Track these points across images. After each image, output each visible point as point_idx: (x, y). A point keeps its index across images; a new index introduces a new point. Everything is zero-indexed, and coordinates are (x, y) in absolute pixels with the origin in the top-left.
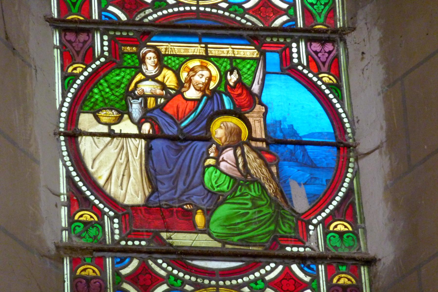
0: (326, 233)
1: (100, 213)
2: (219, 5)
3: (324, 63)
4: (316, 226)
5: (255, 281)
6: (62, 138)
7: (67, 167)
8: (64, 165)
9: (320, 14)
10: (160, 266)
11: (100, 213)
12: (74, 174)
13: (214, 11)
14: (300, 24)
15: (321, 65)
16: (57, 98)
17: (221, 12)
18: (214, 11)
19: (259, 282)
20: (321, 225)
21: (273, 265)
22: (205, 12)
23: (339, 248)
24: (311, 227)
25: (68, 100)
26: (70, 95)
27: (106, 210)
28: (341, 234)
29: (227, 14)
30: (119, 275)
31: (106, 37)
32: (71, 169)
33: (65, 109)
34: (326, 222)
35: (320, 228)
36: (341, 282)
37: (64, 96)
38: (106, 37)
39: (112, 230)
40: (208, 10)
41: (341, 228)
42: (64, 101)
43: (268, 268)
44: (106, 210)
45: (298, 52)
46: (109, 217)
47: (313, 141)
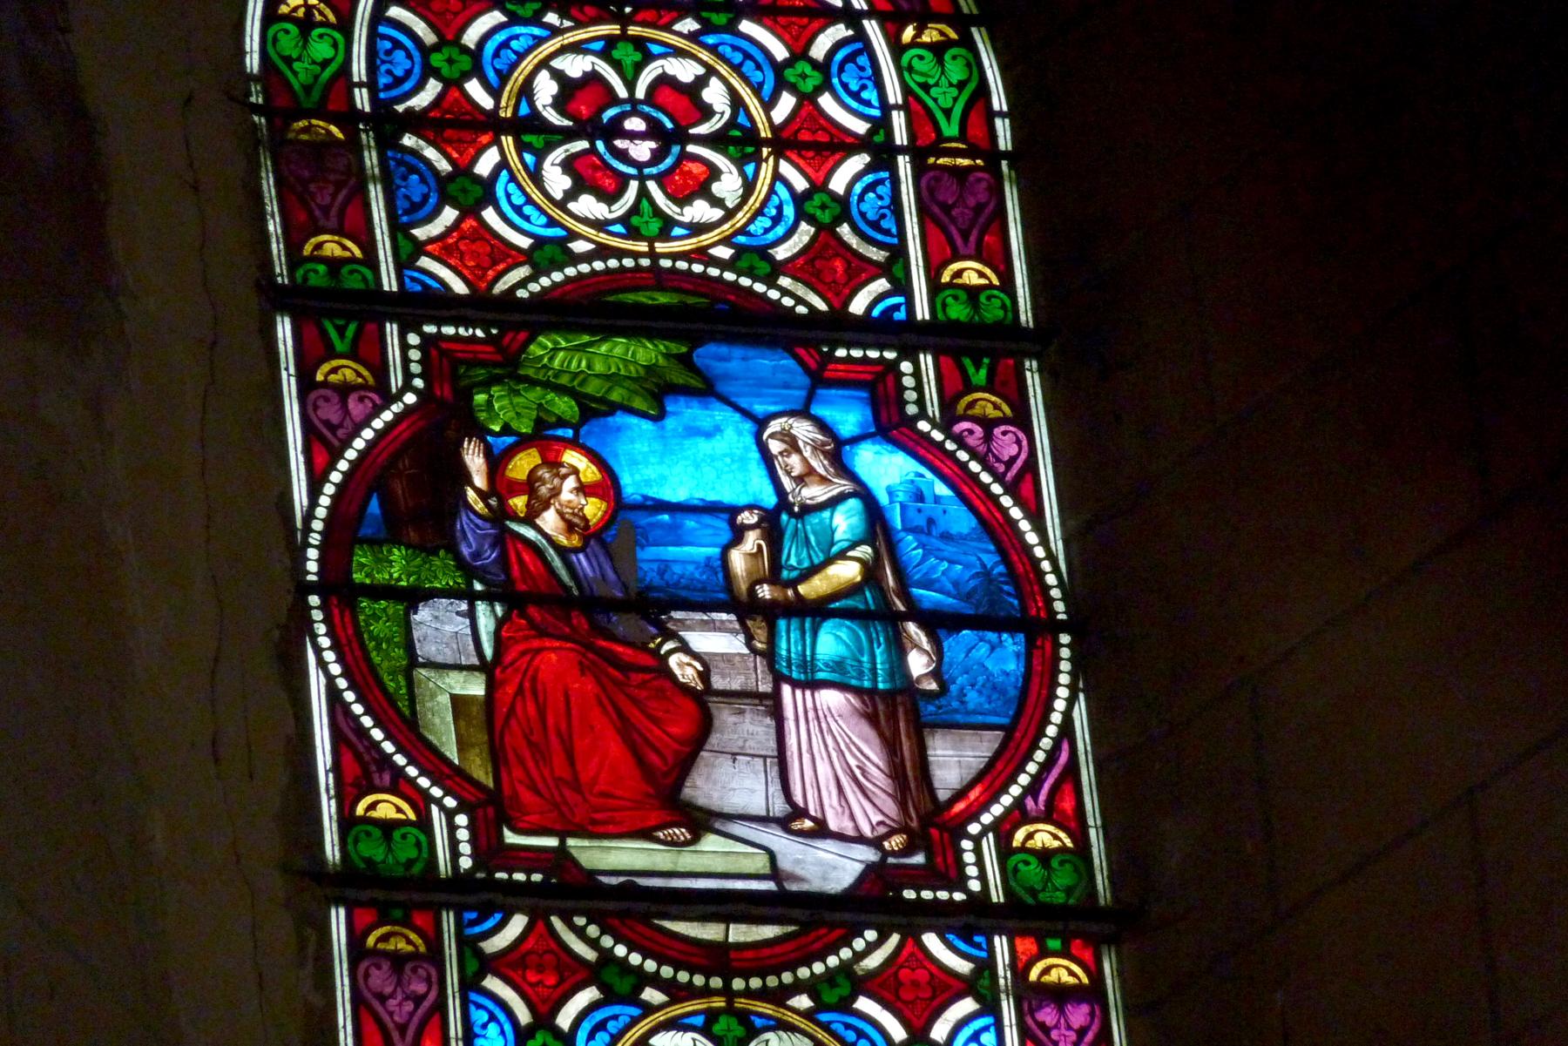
0: (1005, 851)
1: (421, 801)
2: (713, 251)
3: (948, 113)
4: (977, 840)
5: (830, 976)
6: (314, 600)
7: (330, 680)
8: (322, 664)
9: (948, 113)
10: (580, 933)
11: (421, 801)
12: (350, 696)
13: (698, 268)
14: (922, 312)
15: (940, 116)
16: (293, 380)
17: (714, 272)
18: (698, 268)
19: (840, 980)
20: (991, 835)
21: (871, 935)
22: (673, 270)
23: (1039, 892)
24: (967, 844)
25: (325, 501)
26: (329, 489)
27: (436, 792)
28: (1044, 855)
29: (729, 276)
30: (479, 953)
31: (413, 339)
32: (342, 683)
33: (317, 525)
34: (1003, 830)
35: (988, 844)
36: (1052, 977)
37: (314, 492)
38: (413, 339)
39: (454, 843)
40: (682, 265)
41: (971, 278)
42: (313, 503)
43: (859, 944)
44: (436, 792)
45: (980, 863)
46: (442, 808)
47: (915, 193)
